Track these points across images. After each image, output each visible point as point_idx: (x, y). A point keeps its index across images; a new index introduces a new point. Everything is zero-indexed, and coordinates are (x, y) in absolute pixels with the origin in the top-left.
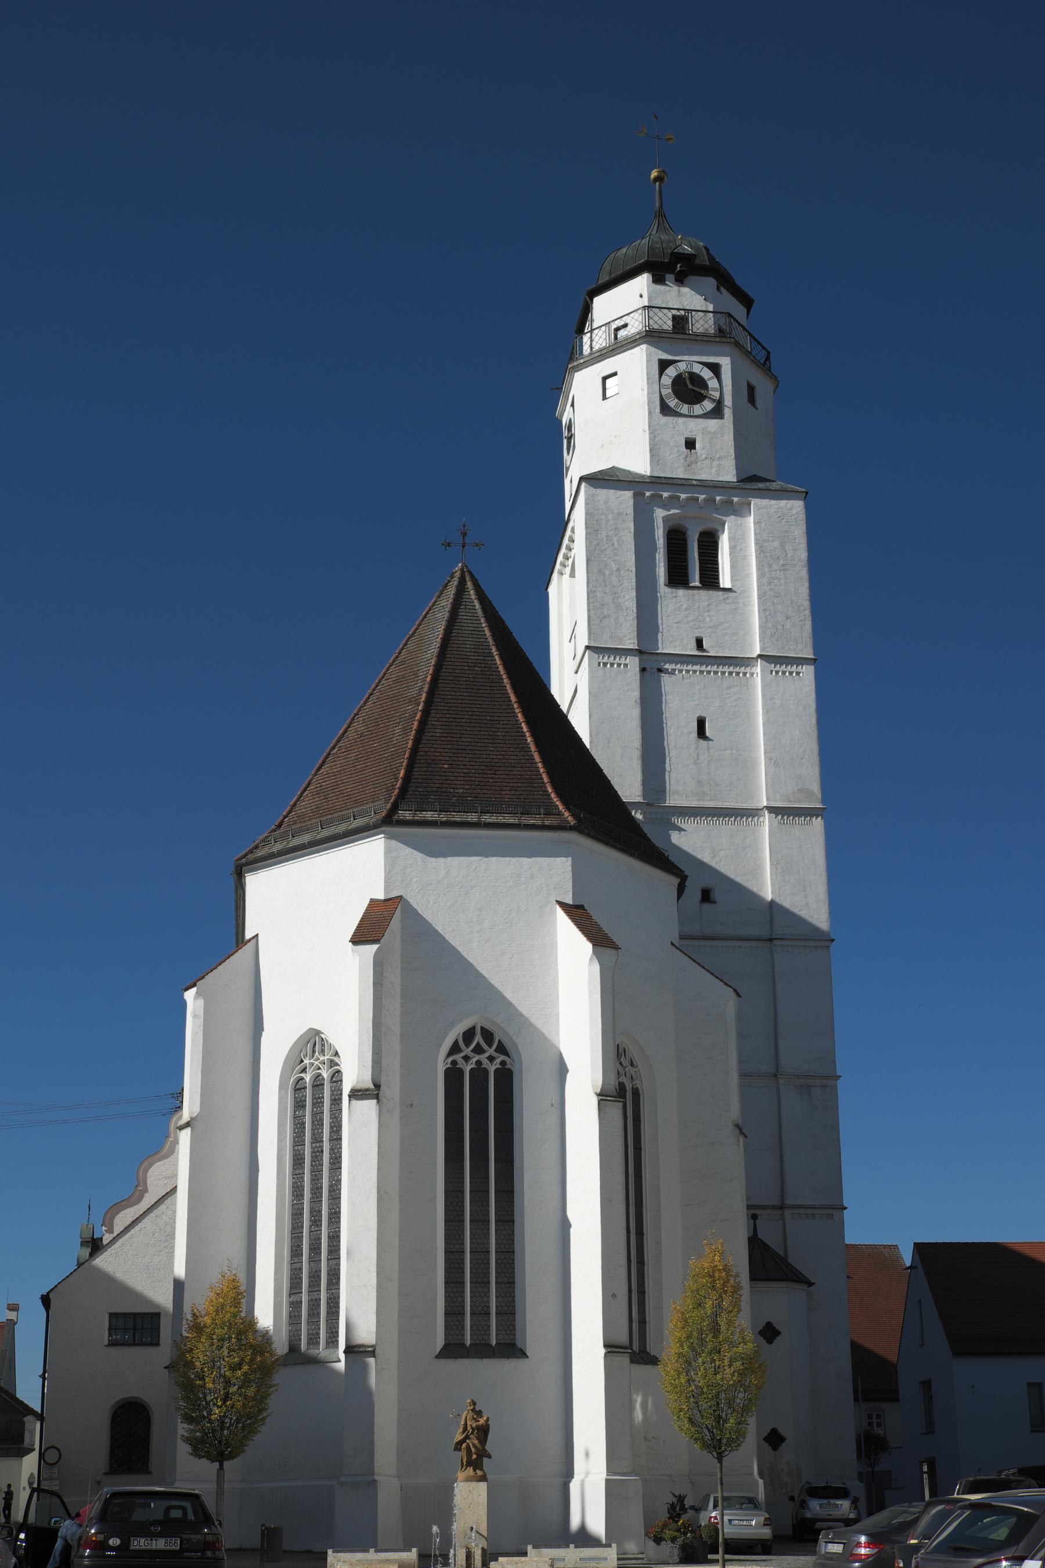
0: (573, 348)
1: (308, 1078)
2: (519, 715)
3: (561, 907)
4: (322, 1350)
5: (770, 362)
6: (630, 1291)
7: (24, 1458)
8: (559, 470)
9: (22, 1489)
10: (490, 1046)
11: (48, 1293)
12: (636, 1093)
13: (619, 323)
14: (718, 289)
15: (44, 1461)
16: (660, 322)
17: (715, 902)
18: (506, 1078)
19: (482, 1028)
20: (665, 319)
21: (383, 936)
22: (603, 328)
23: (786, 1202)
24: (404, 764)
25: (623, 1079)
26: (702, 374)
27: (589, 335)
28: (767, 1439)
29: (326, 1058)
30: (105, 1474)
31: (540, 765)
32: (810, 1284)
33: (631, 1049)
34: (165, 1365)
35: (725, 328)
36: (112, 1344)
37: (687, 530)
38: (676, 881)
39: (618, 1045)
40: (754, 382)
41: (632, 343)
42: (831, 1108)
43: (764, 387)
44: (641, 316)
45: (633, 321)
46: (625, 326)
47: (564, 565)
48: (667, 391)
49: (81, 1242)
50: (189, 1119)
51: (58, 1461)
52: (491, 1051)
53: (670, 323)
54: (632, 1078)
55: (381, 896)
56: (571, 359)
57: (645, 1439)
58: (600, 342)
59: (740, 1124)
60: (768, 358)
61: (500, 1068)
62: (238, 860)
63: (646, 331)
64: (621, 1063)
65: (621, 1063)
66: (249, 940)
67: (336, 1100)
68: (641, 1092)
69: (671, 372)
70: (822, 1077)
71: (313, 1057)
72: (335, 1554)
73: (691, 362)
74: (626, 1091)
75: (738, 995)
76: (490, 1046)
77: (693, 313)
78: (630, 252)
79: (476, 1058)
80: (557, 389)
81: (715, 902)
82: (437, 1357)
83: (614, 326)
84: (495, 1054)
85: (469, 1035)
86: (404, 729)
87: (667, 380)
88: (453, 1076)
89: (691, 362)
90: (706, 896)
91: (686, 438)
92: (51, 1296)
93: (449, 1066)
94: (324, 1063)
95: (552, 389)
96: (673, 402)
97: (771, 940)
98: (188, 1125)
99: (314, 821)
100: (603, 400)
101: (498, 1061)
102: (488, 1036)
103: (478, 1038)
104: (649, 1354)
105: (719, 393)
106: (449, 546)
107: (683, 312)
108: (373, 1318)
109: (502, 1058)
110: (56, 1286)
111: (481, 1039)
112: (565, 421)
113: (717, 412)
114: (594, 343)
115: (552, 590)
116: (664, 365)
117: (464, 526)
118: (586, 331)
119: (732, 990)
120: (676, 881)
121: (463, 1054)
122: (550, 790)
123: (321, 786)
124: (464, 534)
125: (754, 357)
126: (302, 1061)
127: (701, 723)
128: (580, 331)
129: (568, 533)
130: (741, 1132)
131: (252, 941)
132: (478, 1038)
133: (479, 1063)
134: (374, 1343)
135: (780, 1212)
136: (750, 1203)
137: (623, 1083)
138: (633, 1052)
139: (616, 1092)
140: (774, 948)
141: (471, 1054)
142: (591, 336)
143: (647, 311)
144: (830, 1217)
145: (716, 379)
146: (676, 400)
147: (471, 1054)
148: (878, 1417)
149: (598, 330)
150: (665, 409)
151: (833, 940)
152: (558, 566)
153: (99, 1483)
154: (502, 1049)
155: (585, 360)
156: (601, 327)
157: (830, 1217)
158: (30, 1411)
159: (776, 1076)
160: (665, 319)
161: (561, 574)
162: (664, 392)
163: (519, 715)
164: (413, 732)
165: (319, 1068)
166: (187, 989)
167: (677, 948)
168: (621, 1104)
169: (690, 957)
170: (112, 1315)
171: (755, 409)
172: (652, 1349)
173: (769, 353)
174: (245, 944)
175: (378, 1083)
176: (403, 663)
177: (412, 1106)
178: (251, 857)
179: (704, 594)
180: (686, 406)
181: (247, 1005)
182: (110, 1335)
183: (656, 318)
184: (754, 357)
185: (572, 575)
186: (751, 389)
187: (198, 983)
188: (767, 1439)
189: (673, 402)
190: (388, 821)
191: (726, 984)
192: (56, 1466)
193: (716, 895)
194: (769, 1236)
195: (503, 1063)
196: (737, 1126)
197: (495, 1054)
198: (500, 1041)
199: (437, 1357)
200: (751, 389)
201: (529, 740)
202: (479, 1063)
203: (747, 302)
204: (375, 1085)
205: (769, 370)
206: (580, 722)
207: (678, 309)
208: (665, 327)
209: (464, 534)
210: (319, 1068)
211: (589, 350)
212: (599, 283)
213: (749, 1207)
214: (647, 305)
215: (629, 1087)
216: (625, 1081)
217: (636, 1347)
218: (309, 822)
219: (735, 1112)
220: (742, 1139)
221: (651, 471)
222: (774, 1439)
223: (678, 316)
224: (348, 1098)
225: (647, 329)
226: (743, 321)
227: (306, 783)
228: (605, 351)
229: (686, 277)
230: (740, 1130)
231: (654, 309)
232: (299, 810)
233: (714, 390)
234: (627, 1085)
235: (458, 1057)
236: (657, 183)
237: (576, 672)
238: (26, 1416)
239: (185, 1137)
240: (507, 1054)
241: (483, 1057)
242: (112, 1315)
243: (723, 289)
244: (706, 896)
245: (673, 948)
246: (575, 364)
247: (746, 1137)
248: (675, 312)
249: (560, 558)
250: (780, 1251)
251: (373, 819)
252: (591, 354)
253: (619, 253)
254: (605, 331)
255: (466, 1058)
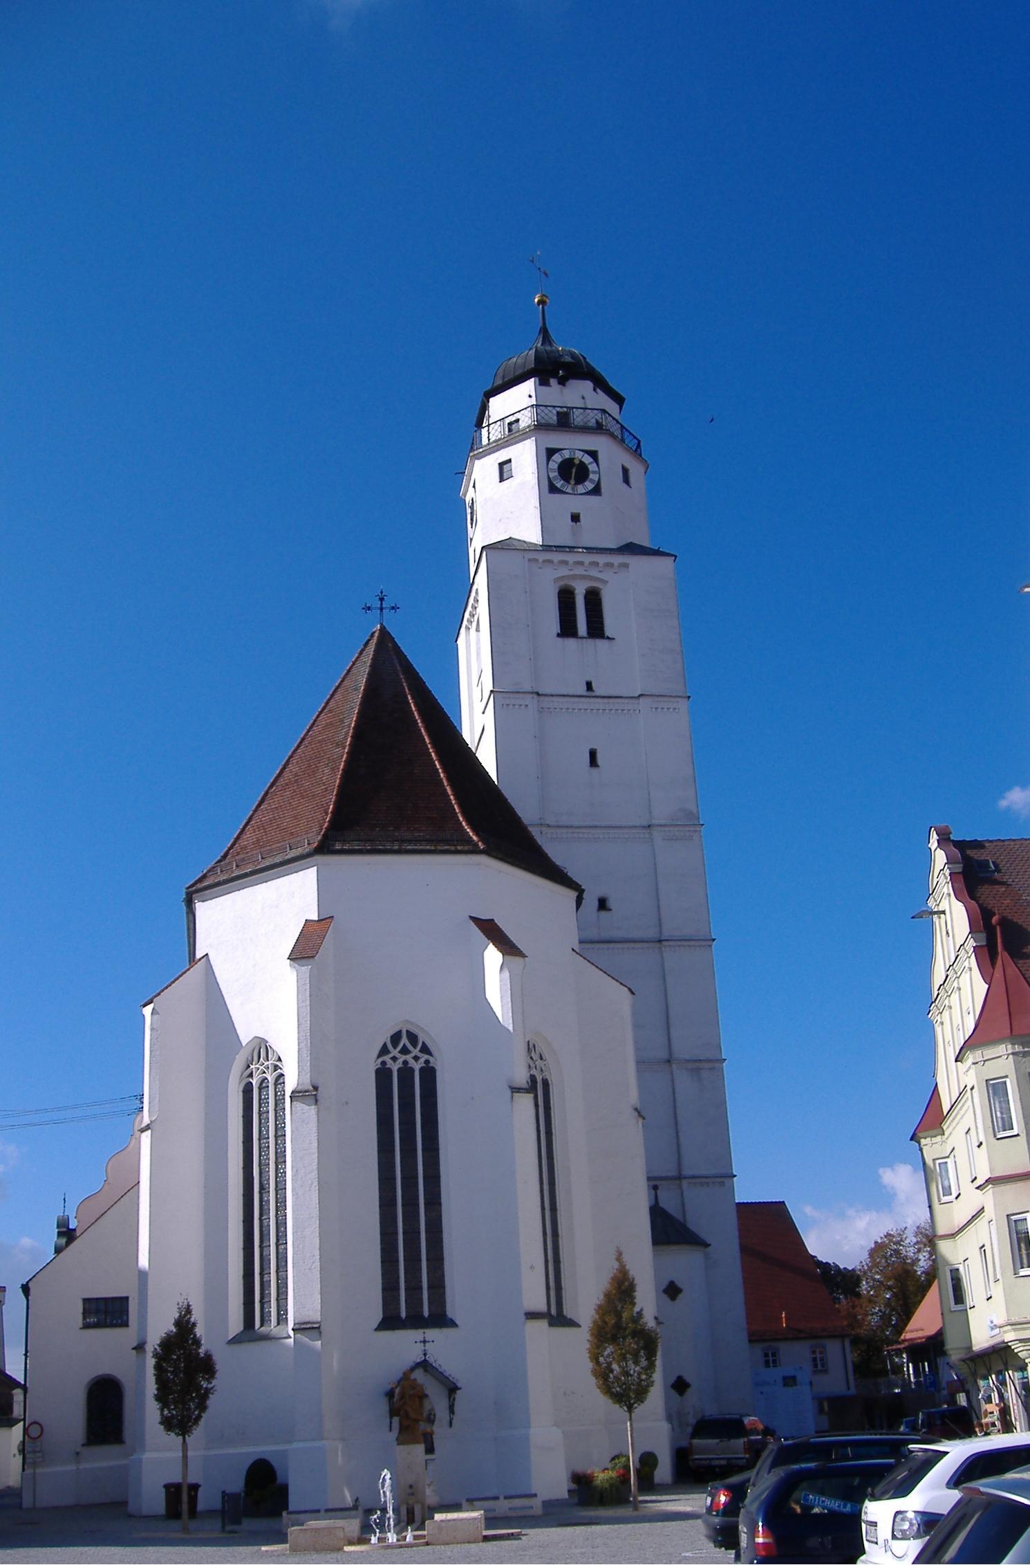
0: (473, 440)
1: (255, 1082)
2: (433, 754)
3: (473, 921)
4: (272, 1327)
5: (640, 450)
6: (546, 1261)
7: (13, 1428)
8: (464, 541)
9: (12, 1456)
10: (415, 1047)
11: (28, 1282)
12: (546, 1083)
13: (512, 419)
14: (595, 390)
15: (28, 1436)
16: (546, 417)
17: (610, 910)
18: (429, 1074)
19: (407, 1031)
20: (550, 414)
21: (317, 953)
22: (499, 423)
23: (683, 1173)
24: (333, 800)
25: (534, 1072)
26: (589, 467)
27: (487, 428)
28: (666, 1291)
29: (270, 1062)
30: (83, 1445)
31: (452, 797)
32: (707, 1245)
33: (540, 1044)
34: (133, 1346)
35: (601, 420)
36: (86, 1326)
37: (575, 589)
38: (574, 894)
39: (529, 1042)
40: (627, 465)
41: (524, 435)
42: (719, 1088)
43: (636, 470)
44: (530, 414)
45: (524, 416)
46: (517, 421)
47: (470, 622)
48: (554, 474)
49: (58, 1232)
50: (149, 1122)
51: (40, 1436)
52: (416, 1052)
53: (555, 418)
54: (542, 1070)
55: (314, 916)
56: (472, 450)
57: (565, 1394)
58: (496, 434)
59: (639, 1108)
60: (639, 446)
61: (424, 1067)
62: (188, 888)
63: (534, 425)
64: (531, 1058)
65: (531, 1058)
66: (200, 959)
67: (279, 1102)
68: (550, 1082)
69: (557, 458)
70: (709, 1061)
71: (258, 1062)
72: (289, 1516)
73: (572, 444)
74: (537, 1082)
75: (633, 993)
76: (415, 1047)
77: (574, 410)
78: (520, 361)
79: (403, 1058)
80: (461, 473)
81: (610, 910)
82: (376, 1330)
83: (507, 421)
84: (420, 1055)
85: (396, 1038)
86: (333, 769)
87: (554, 465)
88: (383, 1075)
89: (572, 444)
90: (603, 904)
91: (572, 513)
92: (30, 1284)
93: (379, 1066)
94: (268, 1068)
95: (456, 474)
96: (559, 484)
97: (660, 941)
98: (148, 1128)
99: (254, 852)
100: (500, 482)
101: (422, 1060)
102: (413, 1038)
103: (404, 1040)
104: (566, 1318)
105: (598, 475)
106: (369, 610)
107: (565, 409)
108: (317, 1297)
109: (426, 1057)
110: (34, 1276)
111: (407, 1040)
112: (468, 499)
113: (596, 491)
114: (491, 435)
115: (461, 642)
116: (551, 452)
117: (382, 592)
118: (484, 425)
119: (626, 989)
120: (574, 894)
121: (391, 1055)
122: (461, 819)
123: (261, 821)
124: (382, 600)
125: (627, 445)
126: (250, 1067)
127: (593, 755)
128: (479, 425)
129: (473, 594)
130: (640, 1115)
131: (202, 960)
132: (404, 1040)
133: (405, 1062)
134: (319, 1320)
135: (678, 1182)
136: (651, 1175)
137: (534, 1076)
138: (542, 1047)
139: (526, 1084)
140: (663, 949)
141: (398, 1055)
142: (488, 430)
143: (535, 409)
144: (722, 1184)
145: (595, 464)
146: (562, 482)
147: (398, 1055)
148: (774, 1355)
149: (494, 425)
150: (553, 489)
151: (714, 940)
152: (465, 622)
153: (78, 1453)
154: (425, 1049)
155: (484, 449)
156: (496, 422)
157: (722, 1184)
158: (16, 1384)
159: (669, 1061)
160: (550, 414)
161: (468, 628)
162: (552, 475)
163: (433, 754)
164: (340, 772)
165: (264, 1072)
166: (145, 1006)
167: (577, 953)
168: (532, 1095)
169: (589, 961)
170: (86, 1301)
171: (629, 488)
172: (568, 1312)
173: (639, 442)
174: (196, 963)
175: (316, 1085)
176: (330, 711)
177: (347, 1103)
178: (199, 886)
179: (591, 643)
180: (556, 466)
181: (495, 681)
182: (84, 1318)
183: (543, 414)
184: (627, 445)
185: (478, 630)
186: (625, 471)
187: (154, 1000)
188: (666, 1291)
189: (559, 484)
190: (324, 848)
191: (621, 984)
192: (39, 1440)
193: (611, 903)
194: (669, 1203)
195: (427, 1062)
196: (636, 1109)
197: (420, 1055)
198: (423, 1043)
199: (376, 1330)
200: (625, 471)
201: (442, 775)
202: (405, 1062)
203: (619, 399)
204: (314, 1087)
205: (641, 455)
206: (487, 758)
207: (561, 407)
208: (551, 422)
209: (382, 600)
210: (264, 1072)
211: (487, 442)
212: (495, 385)
213: (649, 1179)
214: (535, 403)
215: (539, 1079)
216: (535, 1074)
217: (554, 1312)
218: (251, 853)
219: (633, 1097)
220: (641, 1121)
221: (543, 542)
222: (680, 1386)
223: (561, 413)
224: (289, 1099)
225: (536, 423)
226: (617, 417)
227: (247, 818)
228: (500, 442)
229: (567, 380)
230: (639, 1112)
231: (541, 407)
232: (242, 842)
233: (594, 472)
234: (538, 1078)
235: (387, 1058)
236: (541, 306)
237: (483, 713)
238: (14, 1389)
239: (146, 1138)
240: (430, 1053)
241: (409, 1058)
242: (86, 1301)
243: (598, 390)
244: (603, 904)
245: (574, 953)
246: (476, 452)
247: (644, 1119)
248: (558, 409)
249: (467, 615)
250: (679, 1216)
251: (307, 849)
252: (489, 444)
253: (510, 362)
254: (500, 426)
255: (394, 1059)
